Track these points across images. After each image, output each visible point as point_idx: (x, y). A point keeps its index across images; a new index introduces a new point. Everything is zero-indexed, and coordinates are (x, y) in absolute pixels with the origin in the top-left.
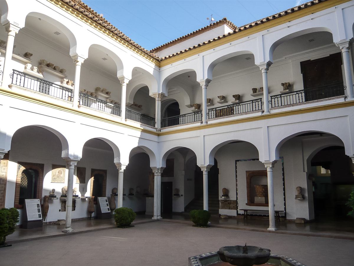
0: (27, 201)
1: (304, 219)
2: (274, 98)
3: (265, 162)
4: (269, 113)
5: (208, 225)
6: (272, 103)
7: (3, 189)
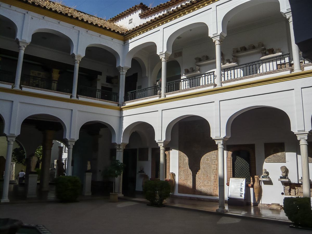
1: (279, 205)
2: (207, 75)
5: (163, 205)
6: (224, 76)
7: (215, 169)
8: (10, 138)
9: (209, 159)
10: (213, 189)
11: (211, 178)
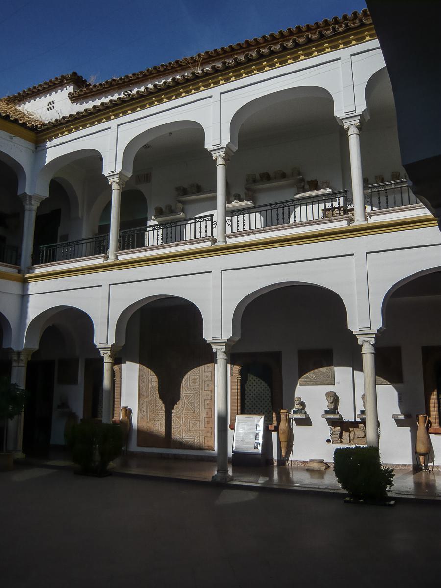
2: (200, 221)
3: (213, 341)
4: (366, 223)
7: (209, 398)
9: (198, 381)
10: (203, 436)
11: (201, 416)
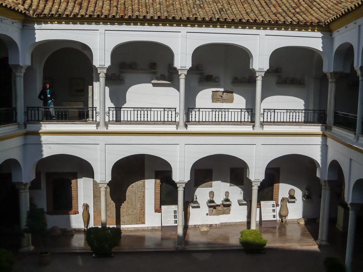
0: (162, 206)
6: (28, 114)
7: (142, 196)
8: (179, 185)
9: (135, 186)
10: (138, 217)
11: (137, 206)
